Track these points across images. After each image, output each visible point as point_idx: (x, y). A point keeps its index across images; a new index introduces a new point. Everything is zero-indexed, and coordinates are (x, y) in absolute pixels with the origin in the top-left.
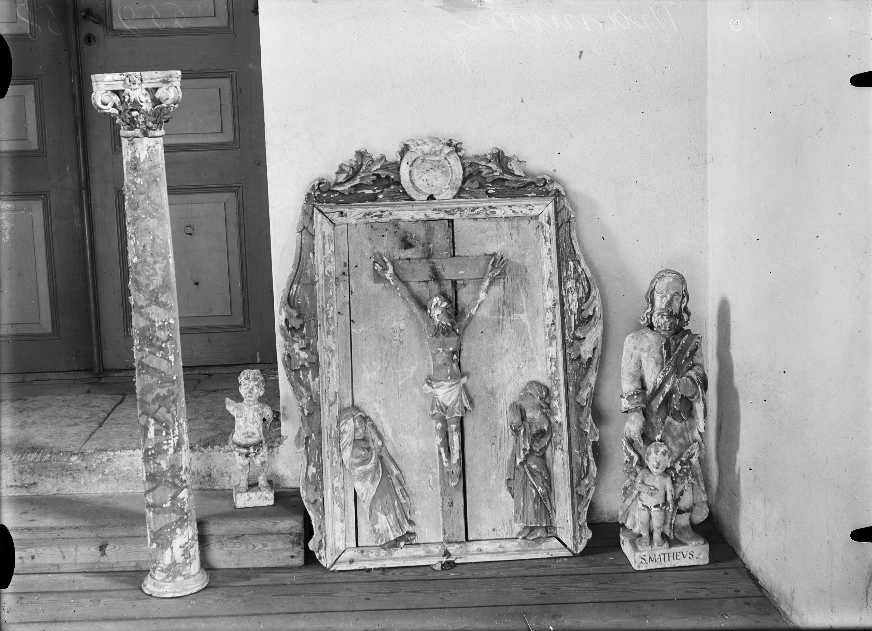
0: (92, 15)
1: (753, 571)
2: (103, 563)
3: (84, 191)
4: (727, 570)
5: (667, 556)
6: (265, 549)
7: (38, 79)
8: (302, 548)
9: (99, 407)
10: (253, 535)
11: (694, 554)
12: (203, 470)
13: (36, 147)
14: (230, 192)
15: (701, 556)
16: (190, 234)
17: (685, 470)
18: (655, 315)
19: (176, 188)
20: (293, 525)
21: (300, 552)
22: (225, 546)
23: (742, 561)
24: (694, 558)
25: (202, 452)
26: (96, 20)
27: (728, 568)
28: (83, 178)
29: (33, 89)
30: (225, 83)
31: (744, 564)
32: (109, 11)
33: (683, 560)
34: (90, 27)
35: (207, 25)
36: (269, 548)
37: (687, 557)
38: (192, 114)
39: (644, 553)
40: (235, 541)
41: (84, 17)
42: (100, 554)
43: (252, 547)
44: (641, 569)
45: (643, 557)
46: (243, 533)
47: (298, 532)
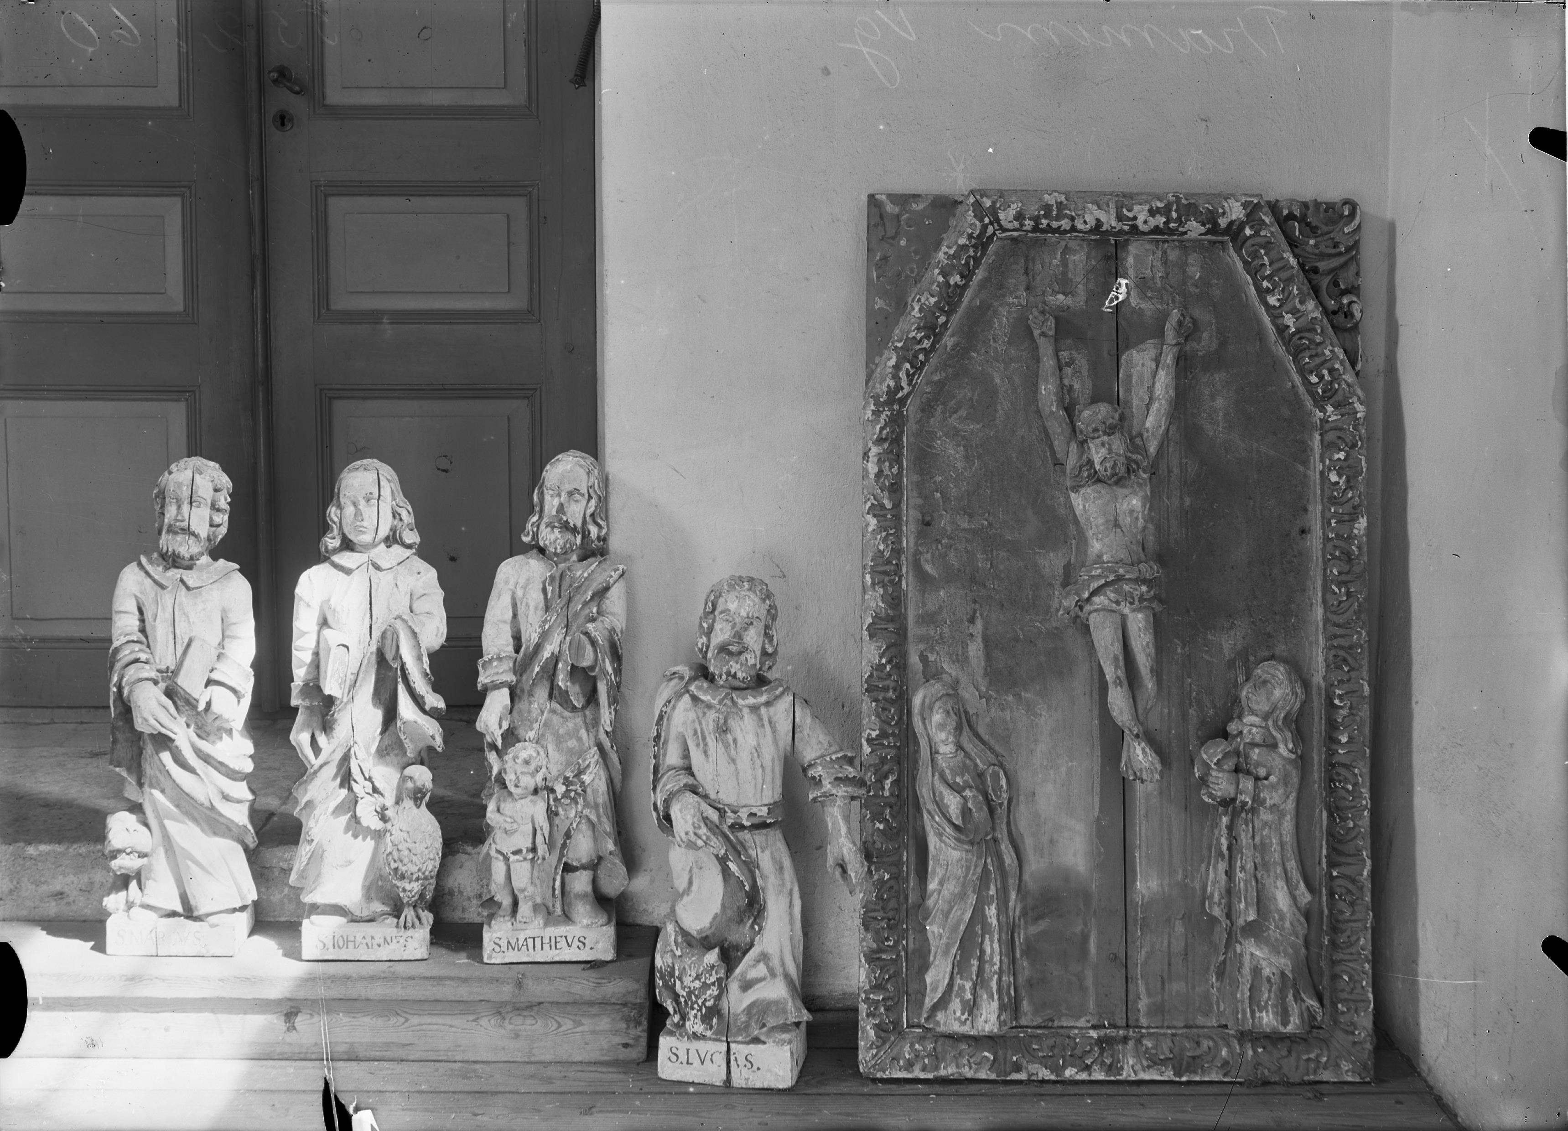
0: (289, 80)
1: (1448, 1099)
2: (290, 1044)
3: (261, 388)
4: (1401, 1097)
5: (538, 941)
6: (578, 1030)
7: (190, 188)
8: (643, 1031)
9: (279, 770)
10: (558, 1003)
11: (586, 941)
12: (469, 889)
13: (180, 308)
14: (518, 398)
15: (600, 946)
16: (446, 471)
17: (572, 794)
18: (542, 527)
19: (423, 387)
20: (630, 989)
21: (640, 1037)
22: (507, 1021)
23: (1426, 1081)
24: (588, 948)
25: (469, 854)
26: (297, 88)
27: (1403, 1093)
28: (260, 365)
29: (179, 206)
30: (518, 206)
31: (1431, 1088)
32: (318, 72)
33: (566, 950)
34: (282, 99)
35: (491, 102)
36: (585, 1028)
37: (575, 945)
38: (458, 257)
39: (499, 935)
40: (525, 1013)
41: (275, 81)
42: (285, 1028)
43: (555, 1025)
44: (493, 961)
45: (497, 941)
46: (541, 1000)
47: (638, 1001)
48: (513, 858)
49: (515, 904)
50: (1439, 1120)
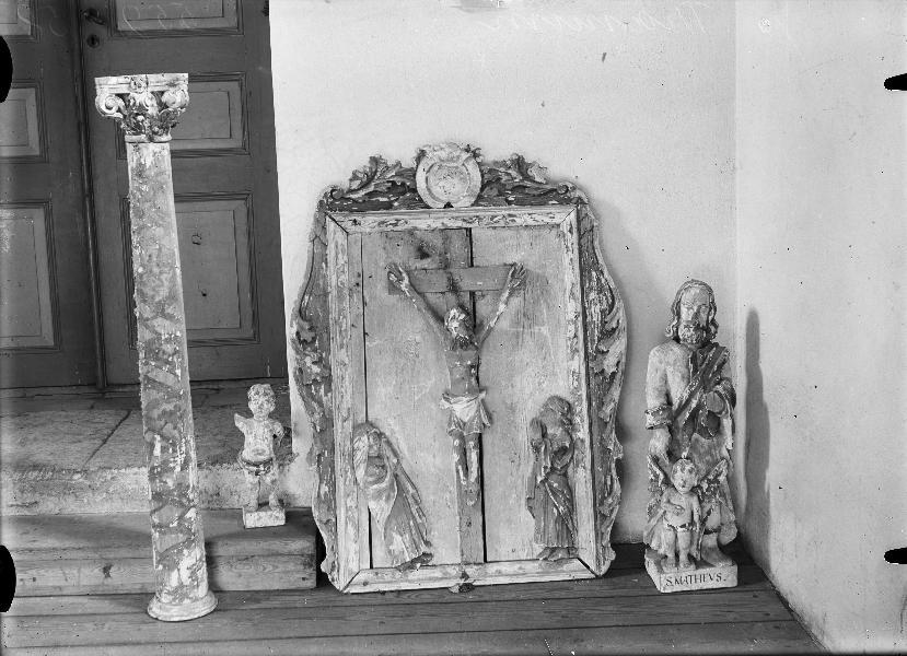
13: (38, 153)
30: (234, 86)
41: (88, 18)
48: (680, 530)
49: (677, 555)
50: (775, 609)
